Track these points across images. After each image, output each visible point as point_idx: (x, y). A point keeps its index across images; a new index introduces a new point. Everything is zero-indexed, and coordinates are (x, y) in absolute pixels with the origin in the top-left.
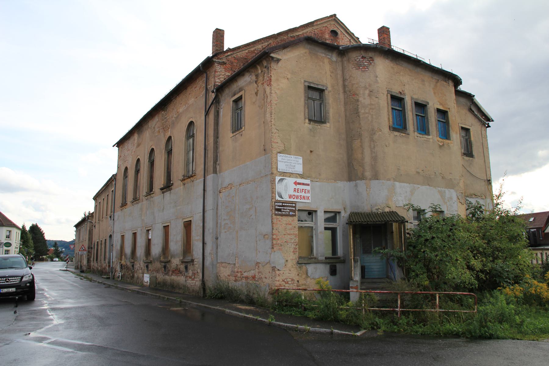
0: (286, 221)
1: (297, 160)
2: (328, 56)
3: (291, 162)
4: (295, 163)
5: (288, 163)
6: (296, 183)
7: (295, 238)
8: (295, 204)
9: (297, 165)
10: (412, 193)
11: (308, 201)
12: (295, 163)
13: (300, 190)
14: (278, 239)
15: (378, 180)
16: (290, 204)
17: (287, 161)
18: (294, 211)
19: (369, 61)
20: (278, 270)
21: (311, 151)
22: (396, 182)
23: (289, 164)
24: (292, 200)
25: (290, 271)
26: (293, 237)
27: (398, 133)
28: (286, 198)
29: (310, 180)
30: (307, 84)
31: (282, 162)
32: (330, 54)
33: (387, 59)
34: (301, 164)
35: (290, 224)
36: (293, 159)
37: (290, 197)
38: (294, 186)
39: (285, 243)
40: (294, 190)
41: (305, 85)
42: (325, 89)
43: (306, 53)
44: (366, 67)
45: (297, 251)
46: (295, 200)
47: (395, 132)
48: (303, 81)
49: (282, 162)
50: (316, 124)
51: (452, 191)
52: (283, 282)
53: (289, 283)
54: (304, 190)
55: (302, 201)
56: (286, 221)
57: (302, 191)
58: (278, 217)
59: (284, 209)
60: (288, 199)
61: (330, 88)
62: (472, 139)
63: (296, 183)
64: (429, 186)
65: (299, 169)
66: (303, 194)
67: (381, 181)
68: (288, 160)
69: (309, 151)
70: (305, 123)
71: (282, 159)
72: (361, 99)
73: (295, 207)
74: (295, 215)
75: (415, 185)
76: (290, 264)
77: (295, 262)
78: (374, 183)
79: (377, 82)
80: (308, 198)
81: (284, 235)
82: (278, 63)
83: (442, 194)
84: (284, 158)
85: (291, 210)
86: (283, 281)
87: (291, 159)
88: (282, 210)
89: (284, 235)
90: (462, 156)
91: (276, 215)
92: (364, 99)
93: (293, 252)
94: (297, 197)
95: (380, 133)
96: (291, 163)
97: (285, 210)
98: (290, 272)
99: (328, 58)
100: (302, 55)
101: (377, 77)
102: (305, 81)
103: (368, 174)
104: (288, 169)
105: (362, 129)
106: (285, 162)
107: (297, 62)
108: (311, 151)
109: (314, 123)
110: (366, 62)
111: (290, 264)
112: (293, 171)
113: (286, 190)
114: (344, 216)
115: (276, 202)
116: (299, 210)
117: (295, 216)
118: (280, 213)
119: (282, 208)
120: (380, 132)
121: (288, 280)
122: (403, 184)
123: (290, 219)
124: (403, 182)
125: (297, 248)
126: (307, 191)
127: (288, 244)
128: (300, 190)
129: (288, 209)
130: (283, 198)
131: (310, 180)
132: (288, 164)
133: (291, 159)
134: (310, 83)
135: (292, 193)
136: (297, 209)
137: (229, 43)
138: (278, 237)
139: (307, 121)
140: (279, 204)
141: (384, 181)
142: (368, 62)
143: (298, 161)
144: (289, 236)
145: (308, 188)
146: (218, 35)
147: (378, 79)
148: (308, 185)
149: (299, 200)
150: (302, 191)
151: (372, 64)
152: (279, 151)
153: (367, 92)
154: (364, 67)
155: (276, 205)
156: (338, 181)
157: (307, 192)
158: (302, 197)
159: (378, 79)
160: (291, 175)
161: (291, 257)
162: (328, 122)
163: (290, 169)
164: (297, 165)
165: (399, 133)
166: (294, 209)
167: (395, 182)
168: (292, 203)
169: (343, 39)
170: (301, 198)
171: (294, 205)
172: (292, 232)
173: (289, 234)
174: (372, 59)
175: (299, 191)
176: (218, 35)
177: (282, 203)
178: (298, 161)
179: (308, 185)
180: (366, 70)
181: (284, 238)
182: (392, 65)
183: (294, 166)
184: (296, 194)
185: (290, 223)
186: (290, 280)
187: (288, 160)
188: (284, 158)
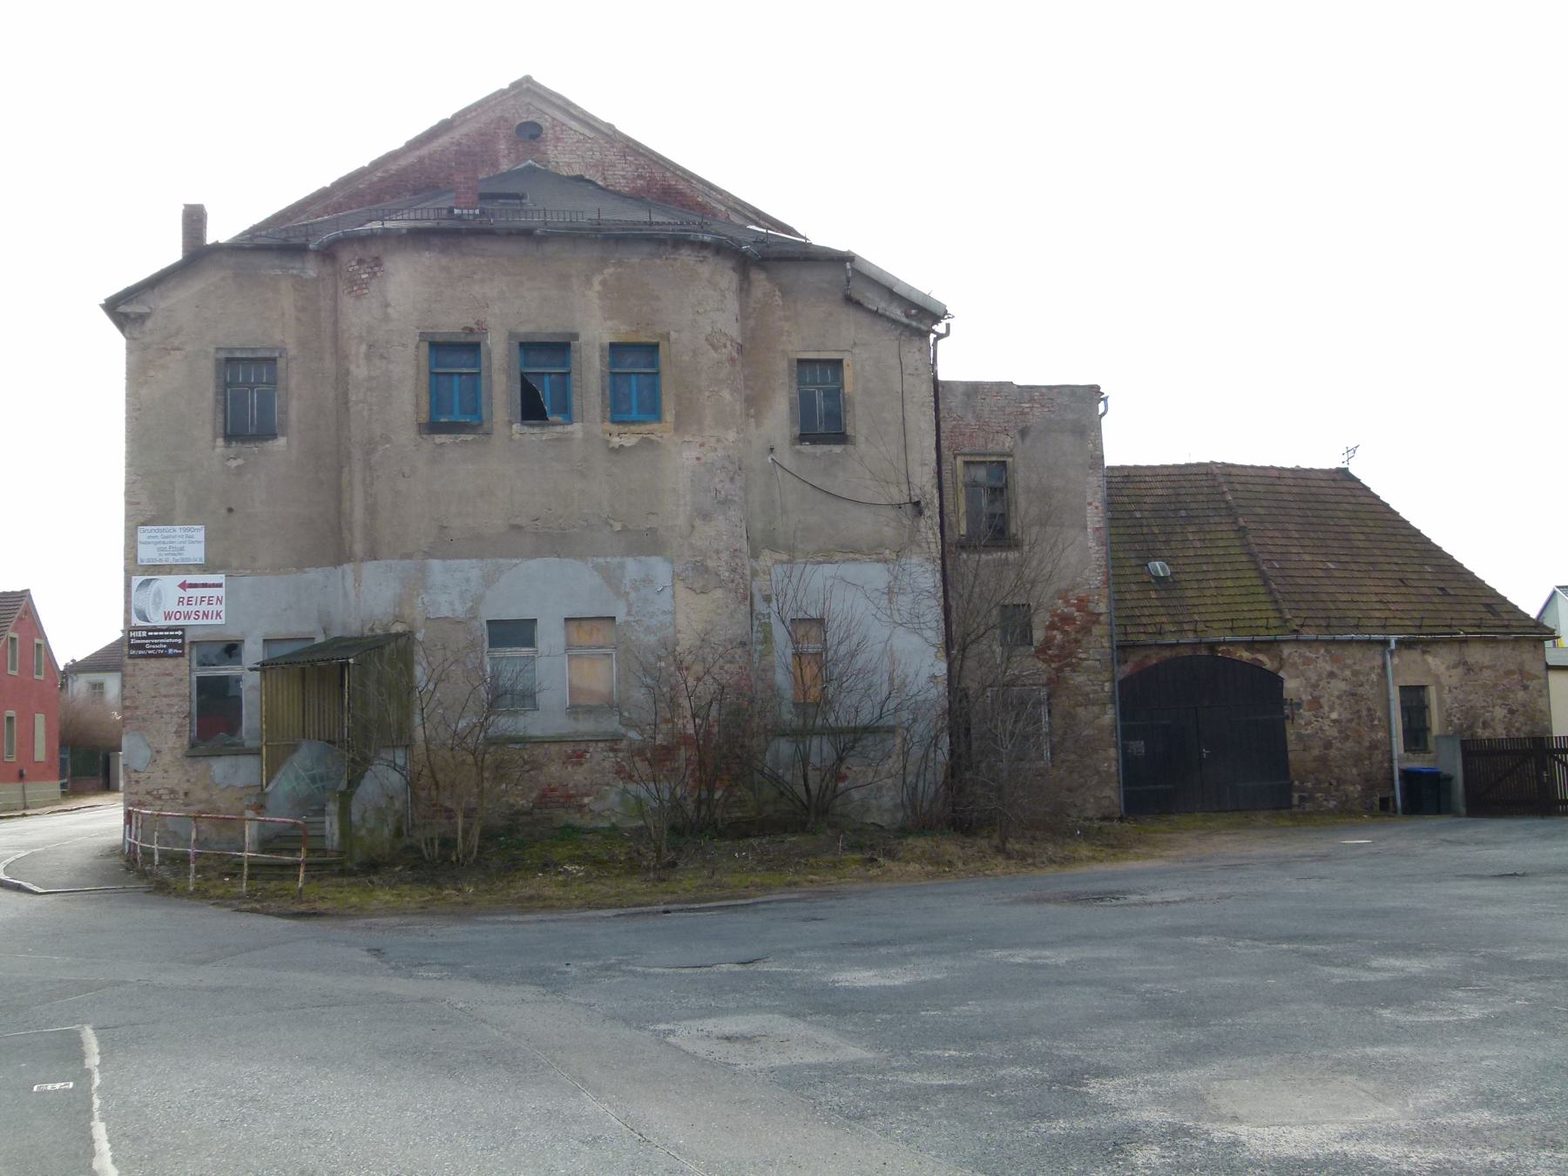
0: (158, 668)
1: (190, 534)
2: (291, 271)
3: (172, 540)
4: (184, 542)
5: (164, 543)
6: (183, 586)
7: (180, 703)
8: (183, 630)
9: (187, 546)
10: (489, 580)
11: (218, 622)
12: (184, 542)
13: (194, 600)
14: (136, 708)
15: (376, 559)
16: (166, 630)
17: (162, 540)
18: (181, 646)
19: (372, 268)
20: (136, 771)
21: (230, 510)
22: (430, 560)
23: (167, 546)
24: (173, 622)
25: (166, 772)
26: (176, 700)
27: (449, 436)
28: (158, 620)
29: (224, 575)
30: (223, 355)
31: (149, 543)
32: (298, 264)
33: (428, 249)
34: (200, 542)
35: (168, 675)
36: (178, 533)
37: (168, 616)
38: (181, 593)
39: (155, 715)
40: (179, 602)
41: (217, 360)
42: (277, 355)
43: (223, 279)
44: (364, 286)
45: (186, 731)
46: (182, 622)
47: (436, 436)
48: (212, 350)
49: (149, 543)
50: (247, 446)
51: (653, 560)
52: (147, 796)
53: (163, 797)
54: (206, 599)
55: (200, 622)
56: (158, 668)
57: (202, 601)
58: (138, 661)
59: (151, 644)
60: (162, 622)
61: (293, 351)
62: (848, 388)
63: (183, 586)
64: (559, 556)
65: (195, 551)
66: (204, 607)
67: (382, 562)
68: (165, 537)
69: (223, 511)
70: (214, 448)
71: (149, 537)
72: (352, 367)
73: (182, 637)
74: (182, 655)
75: (502, 561)
76: (166, 758)
77: (179, 753)
78: (369, 567)
79: (387, 318)
80: (218, 614)
81: (153, 697)
82: (143, 322)
83: (611, 578)
84: (153, 534)
85: (170, 645)
86: (148, 793)
87: (173, 534)
88: (148, 646)
89: (153, 697)
90: (793, 444)
91: (131, 657)
92: (358, 367)
93: (175, 732)
94: (187, 616)
95: (387, 446)
96: (173, 542)
97: (154, 647)
98: (165, 775)
99: (293, 276)
100: (212, 288)
101: (387, 305)
102: (218, 349)
103: (358, 548)
104: (164, 557)
105: (352, 441)
106: (156, 543)
107: (197, 307)
108: (230, 510)
109: (239, 444)
110: (365, 273)
111: (166, 758)
112: (177, 560)
113: (157, 605)
114: (253, 652)
115: (133, 631)
116: (192, 643)
117: (183, 656)
118: (141, 652)
119: (147, 641)
120: (388, 443)
121: (161, 792)
122: (455, 563)
123: (168, 664)
124: (457, 556)
125: (185, 725)
126: (215, 599)
127: (162, 717)
128: (194, 600)
129: (163, 643)
130: (148, 621)
131: (224, 575)
132: (165, 546)
133: (173, 534)
134: (231, 350)
135: (172, 606)
136: (187, 641)
137: (219, 231)
138: (137, 703)
139: (220, 442)
140: (139, 634)
141: (389, 562)
142: (369, 270)
143: (192, 537)
144: (164, 699)
145: (221, 592)
146: (194, 219)
147: (390, 310)
148: (220, 586)
149: (192, 622)
150: (202, 601)
151: (379, 274)
152: (142, 521)
153: (363, 348)
154: (364, 285)
155: (133, 638)
156: (306, 569)
157: (214, 602)
158: (201, 614)
159: (390, 310)
160: (169, 569)
161: (170, 744)
162: (283, 435)
163: (171, 558)
164: (187, 546)
165: (453, 436)
166: (180, 641)
167: (426, 561)
168: (176, 628)
169: (558, 139)
170: (199, 616)
171: (180, 633)
172: (173, 691)
173: (165, 696)
174: (378, 261)
175: (194, 603)
176: (194, 219)
177: (148, 631)
178: (192, 537)
179: (220, 586)
180: (366, 291)
181: (153, 704)
182: (444, 261)
183: (182, 549)
184: (185, 608)
185: (167, 672)
186: (166, 791)
187: (165, 537)
188: (153, 534)
